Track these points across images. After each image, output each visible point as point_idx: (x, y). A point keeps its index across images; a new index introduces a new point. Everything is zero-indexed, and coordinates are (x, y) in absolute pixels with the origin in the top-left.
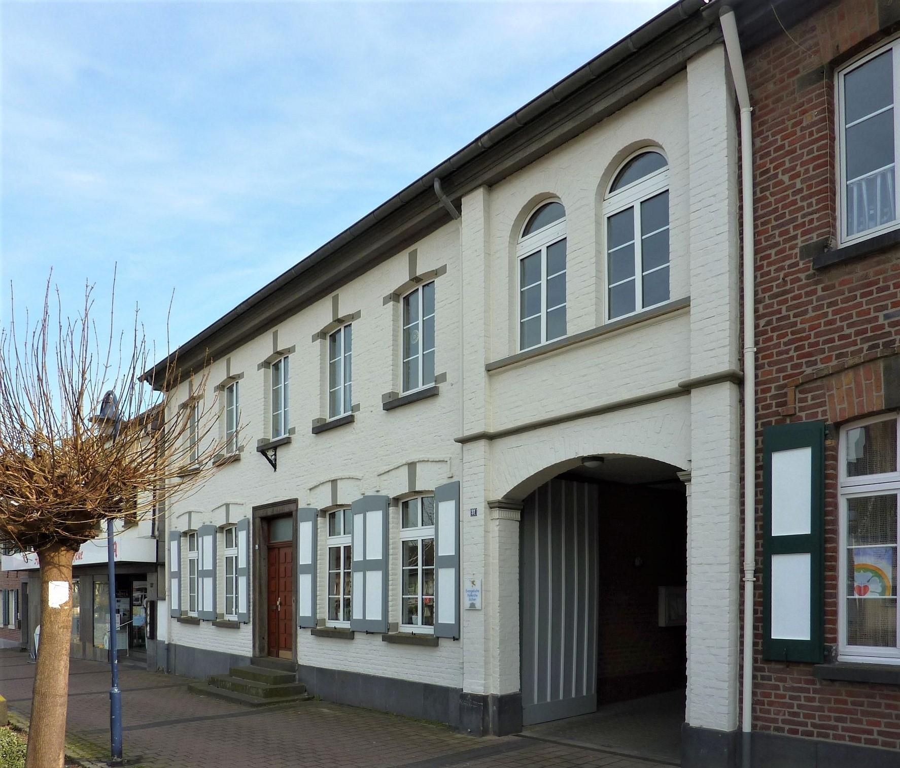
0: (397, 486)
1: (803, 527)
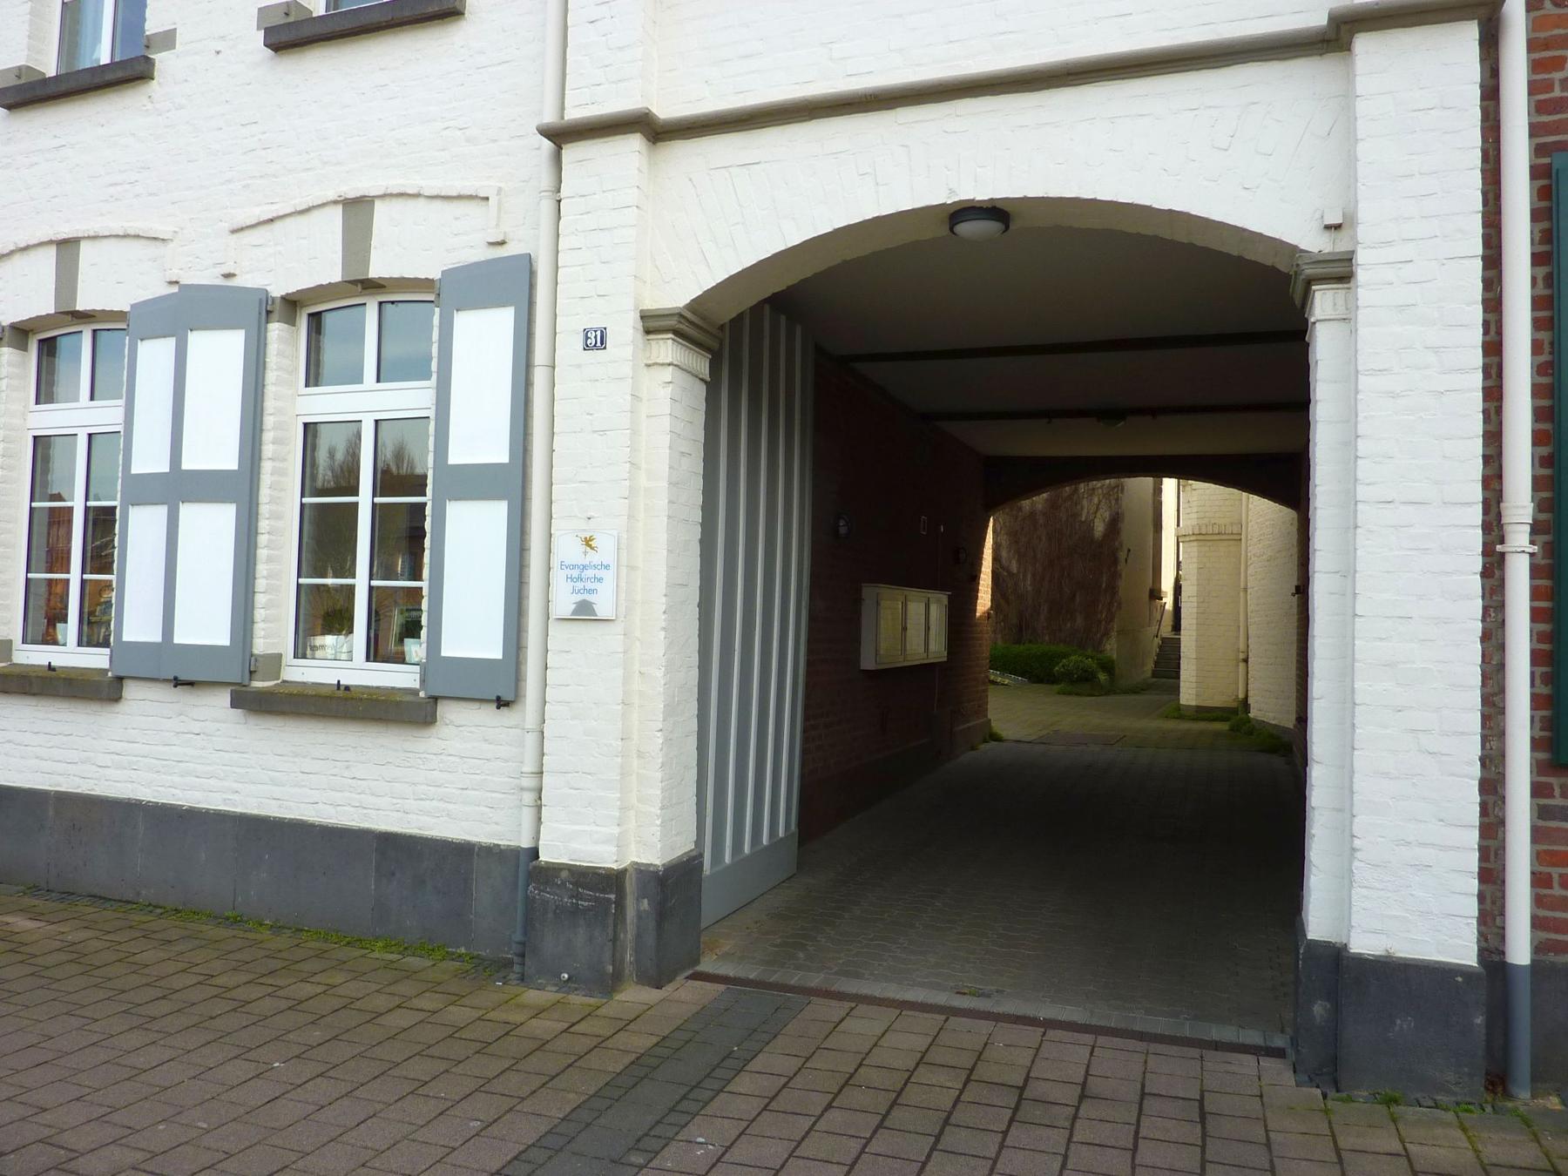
0: (309, 259)
1: (498, 452)
